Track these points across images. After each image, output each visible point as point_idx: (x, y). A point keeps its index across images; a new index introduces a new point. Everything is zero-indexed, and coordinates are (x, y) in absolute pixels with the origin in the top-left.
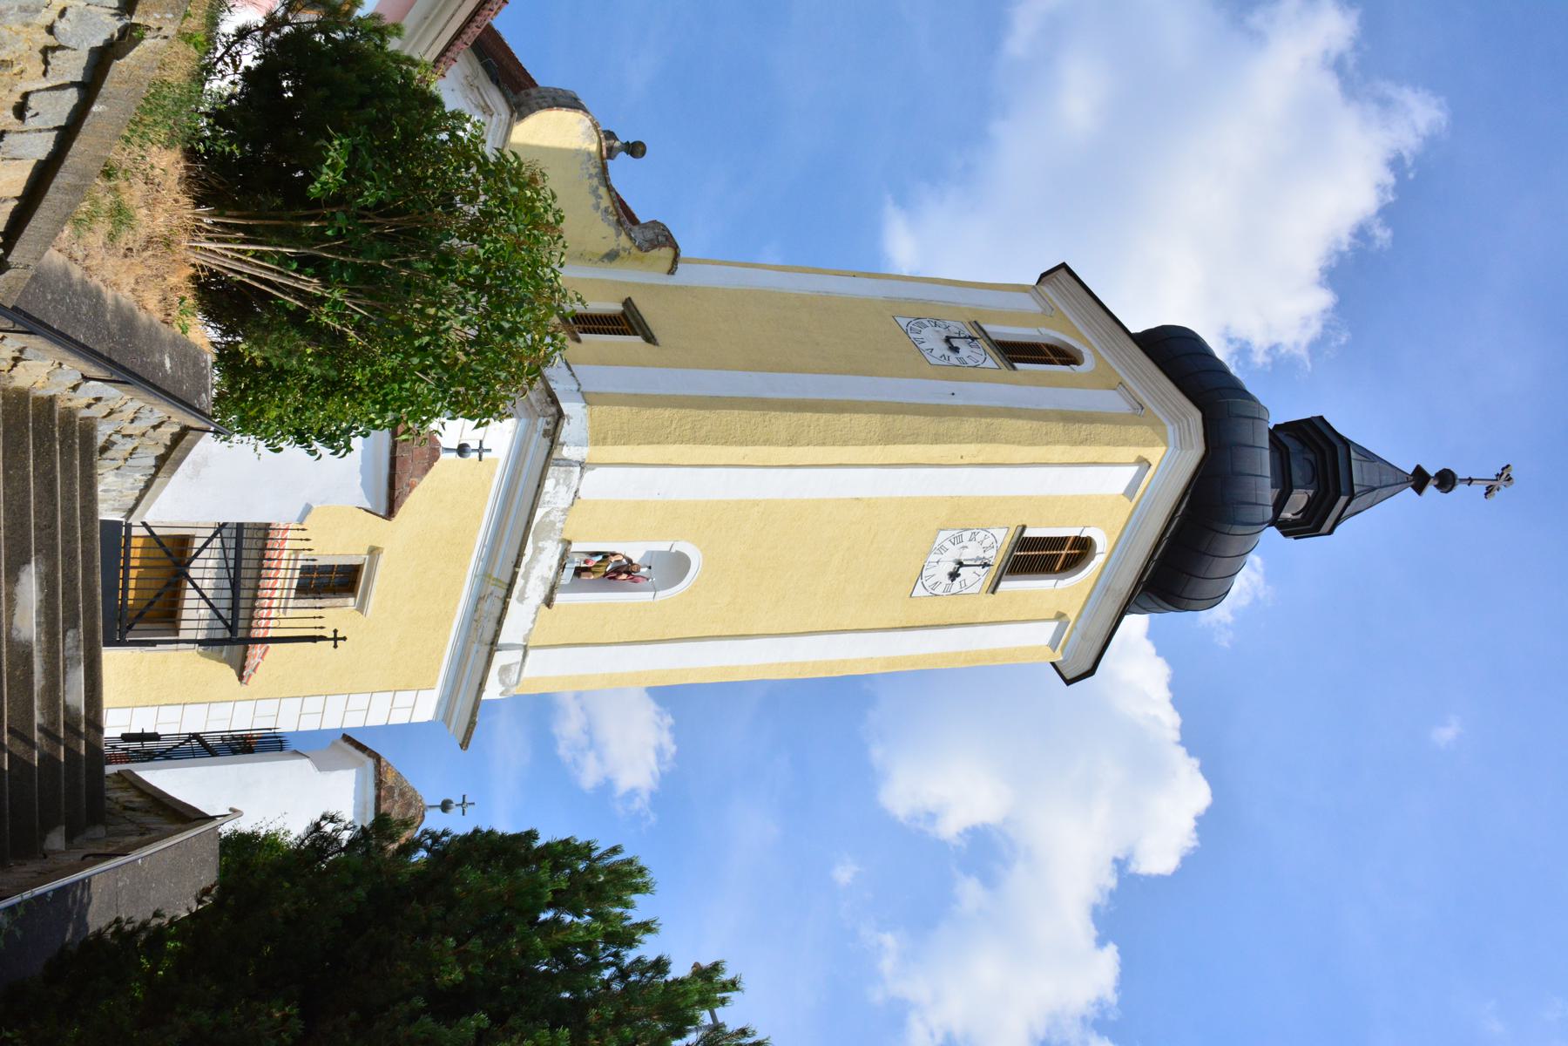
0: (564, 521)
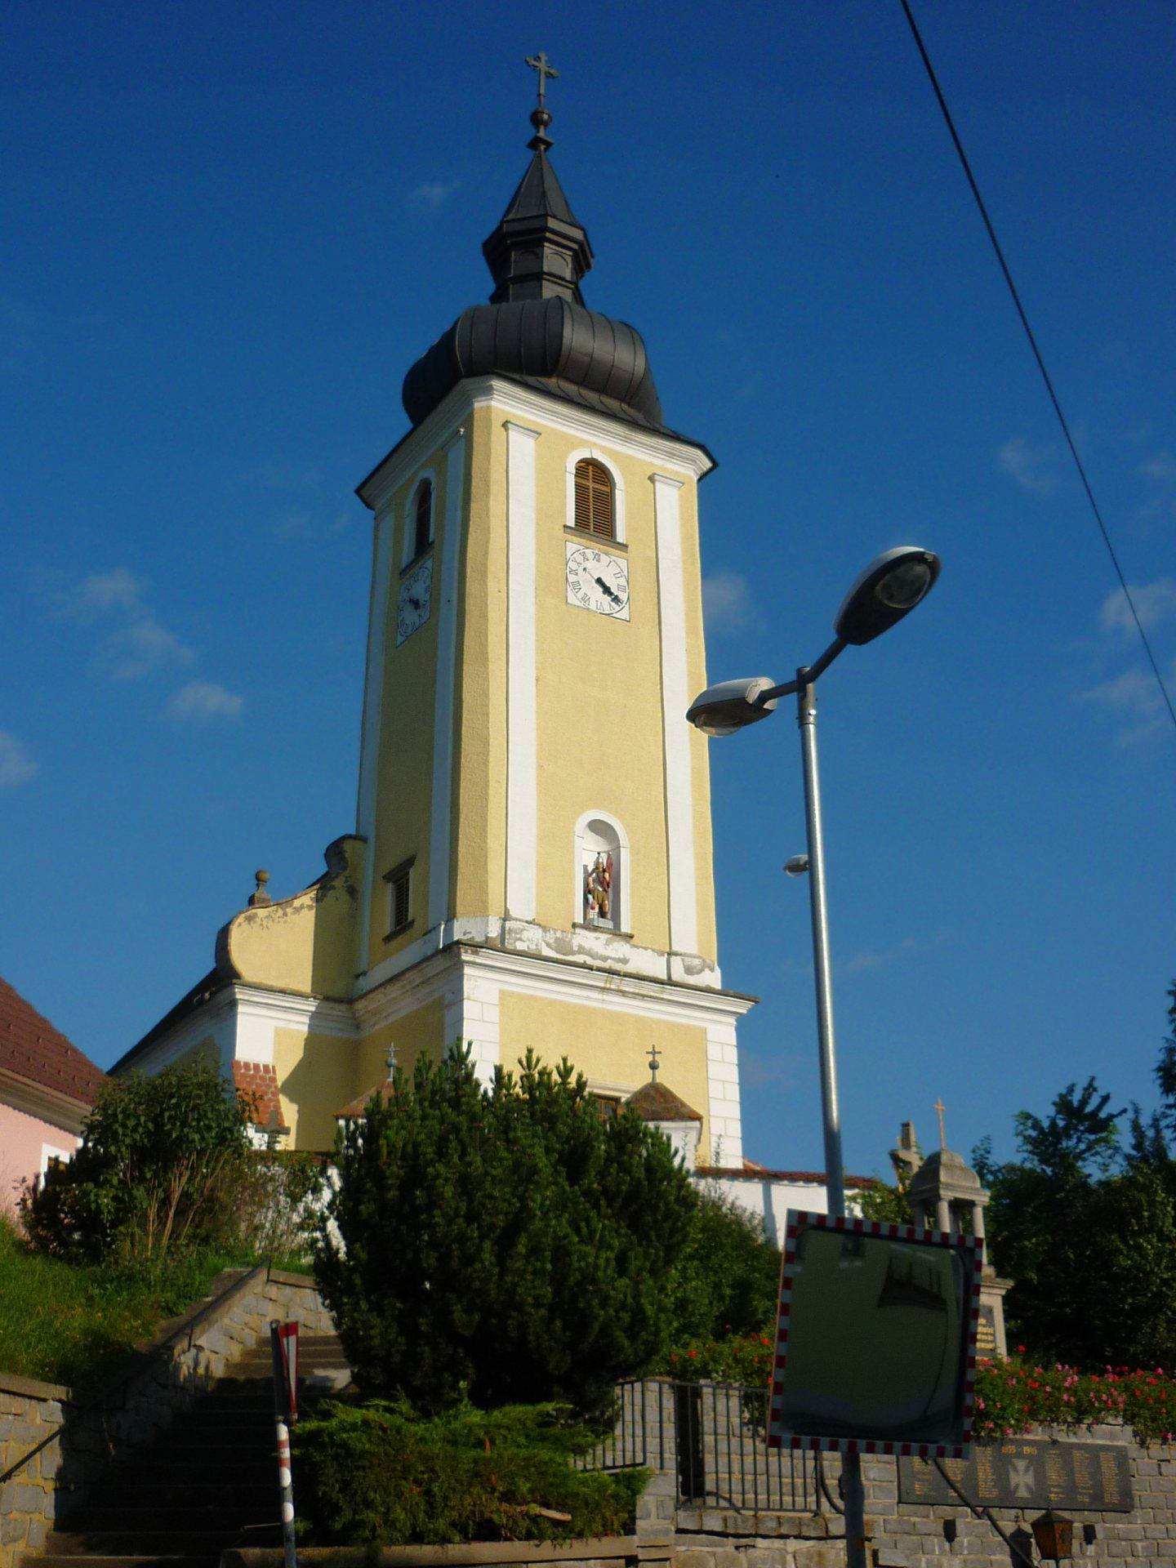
0: (555, 930)
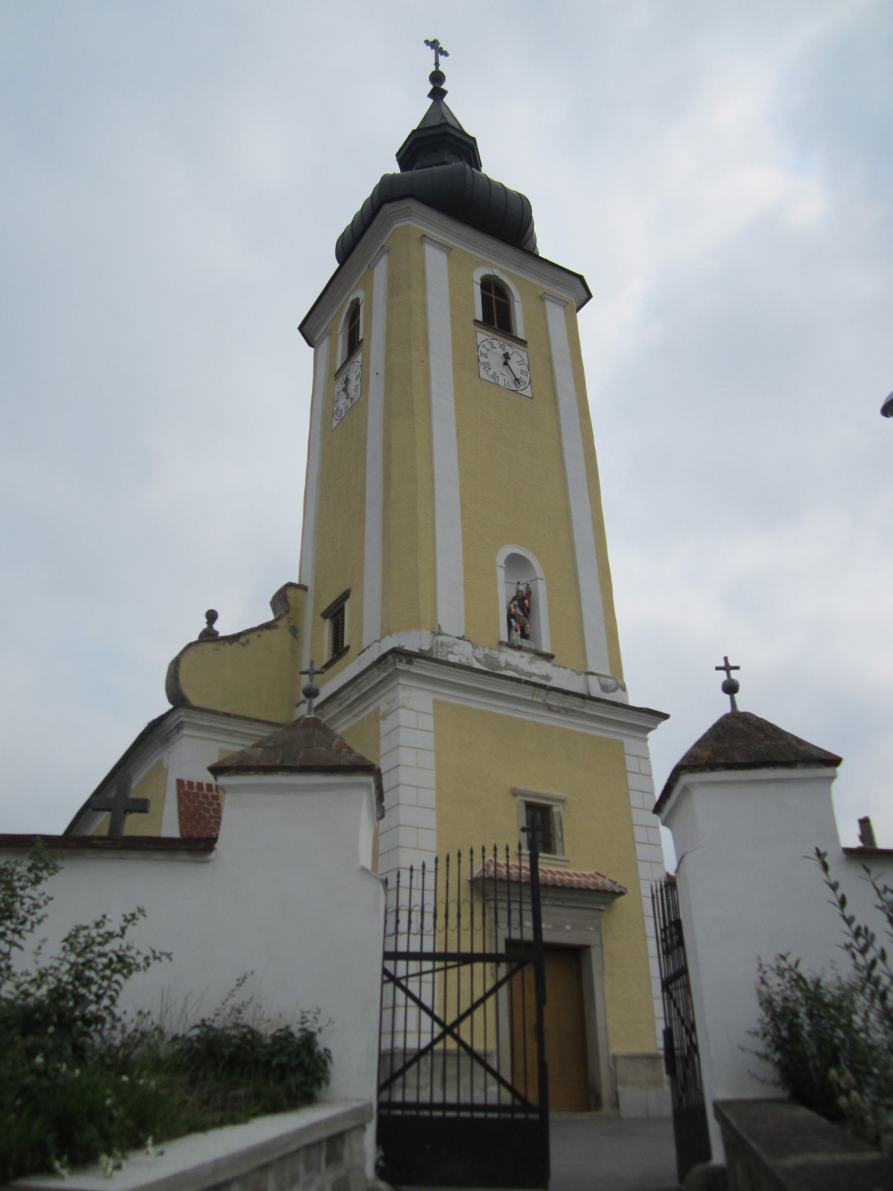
0: (483, 647)
